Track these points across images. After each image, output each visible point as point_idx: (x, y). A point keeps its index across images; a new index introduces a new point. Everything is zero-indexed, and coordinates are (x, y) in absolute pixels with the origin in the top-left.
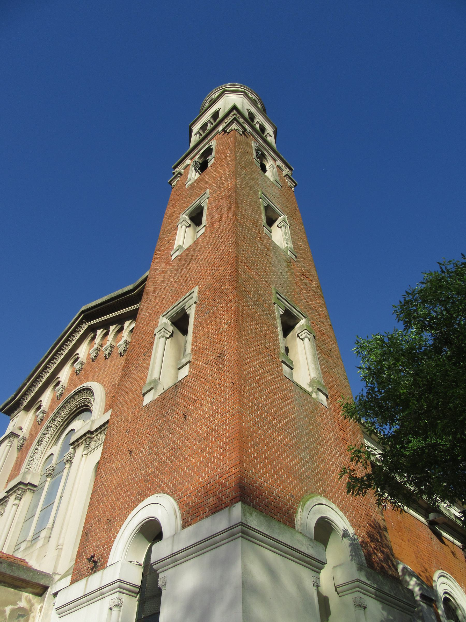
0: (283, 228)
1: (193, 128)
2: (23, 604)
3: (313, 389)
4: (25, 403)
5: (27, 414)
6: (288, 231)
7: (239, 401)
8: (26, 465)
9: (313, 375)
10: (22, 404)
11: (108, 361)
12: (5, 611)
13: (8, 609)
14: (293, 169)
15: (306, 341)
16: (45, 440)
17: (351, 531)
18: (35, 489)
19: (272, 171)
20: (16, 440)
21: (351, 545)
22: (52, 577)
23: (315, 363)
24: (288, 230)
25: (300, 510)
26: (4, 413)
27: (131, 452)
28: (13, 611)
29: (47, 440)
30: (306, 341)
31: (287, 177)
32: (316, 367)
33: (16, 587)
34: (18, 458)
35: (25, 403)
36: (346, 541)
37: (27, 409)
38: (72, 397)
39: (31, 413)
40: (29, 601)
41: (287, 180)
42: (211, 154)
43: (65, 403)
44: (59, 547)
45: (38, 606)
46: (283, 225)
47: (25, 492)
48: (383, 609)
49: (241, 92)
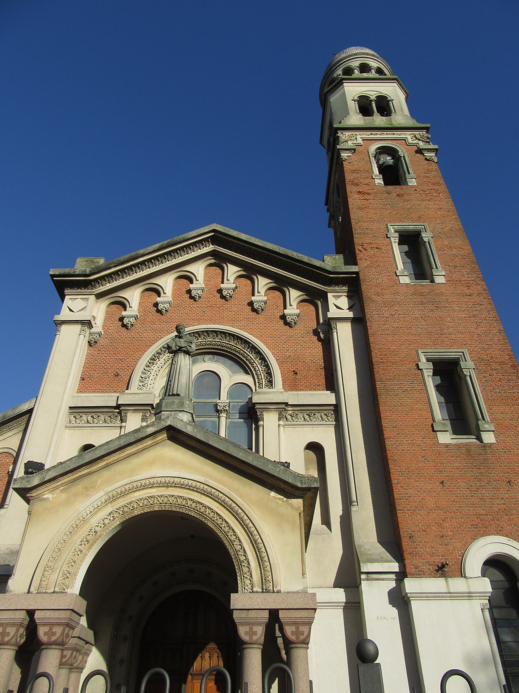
5: (97, 302)
10: (94, 287)
37: (99, 296)
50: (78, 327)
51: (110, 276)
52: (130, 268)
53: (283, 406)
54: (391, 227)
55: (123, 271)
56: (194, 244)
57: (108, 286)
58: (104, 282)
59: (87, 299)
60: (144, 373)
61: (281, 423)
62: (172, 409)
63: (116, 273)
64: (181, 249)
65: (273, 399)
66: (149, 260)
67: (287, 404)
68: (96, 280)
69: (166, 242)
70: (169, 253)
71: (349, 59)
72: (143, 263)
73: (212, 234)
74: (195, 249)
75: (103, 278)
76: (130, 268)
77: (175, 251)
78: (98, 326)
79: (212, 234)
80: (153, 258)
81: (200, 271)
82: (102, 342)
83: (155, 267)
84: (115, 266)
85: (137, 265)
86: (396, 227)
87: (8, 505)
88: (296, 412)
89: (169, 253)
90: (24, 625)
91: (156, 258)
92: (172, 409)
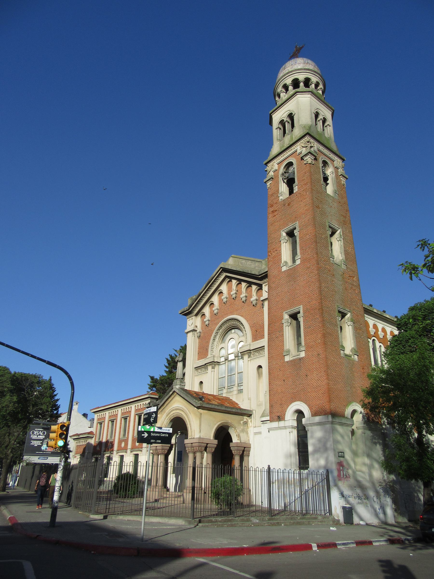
0: (339, 241)
1: (273, 116)
2: (245, 420)
3: (352, 354)
4: (195, 312)
5: (197, 318)
6: (342, 244)
7: (328, 379)
8: (210, 351)
9: (353, 346)
10: (193, 312)
11: (246, 305)
12: (241, 423)
13: (242, 422)
14: (345, 159)
15: (350, 327)
16: (217, 340)
17: (363, 411)
18: (219, 363)
19: (332, 176)
20: (196, 333)
21: (362, 416)
22: (252, 411)
23: (354, 339)
24: (342, 244)
25: (347, 410)
26: (182, 315)
27: (284, 381)
28: (243, 422)
29: (218, 339)
30: (350, 327)
31: (341, 176)
32: (354, 341)
33: (242, 415)
34: (199, 342)
35: (195, 312)
36: (361, 415)
37: (196, 315)
38: (228, 320)
39: (199, 318)
40: (246, 419)
41: (341, 178)
42: (294, 182)
43: (224, 322)
44: (249, 399)
45: (250, 420)
46: (340, 240)
47: (215, 365)
48: (371, 433)
49: (309, 92)
50: (191, 333)
51: (195, 306)
52: (200, 299)
53: (249, 351)
54: (283, 232)
55: (199, 301)
56: (218, 277)
57: (197, 309)
58: (195, 309)
59: (192, 319)
60: (212, 347)
61: (249, 359)
62: (338, 266)
63: (197, 303)
64: (214, 281)
65: (245, 349)
66: (205, 293)
67: (250, 350)
68: (192, 310)
69: (205, 285)
70: (211, 286)
71: (278, 84)
72: (204, 295)
73: (222, 269)
74: (212, 287)
75: (194, 308)
76: (200, 299)
77: (212, 283)
78: (199, 329)
79: (222, 269)
80: (206, 291)
81: (225, 287)
82: (202, 335)
83: (209, 294)
84: (195, 302)
85: (202, 297)
86: (285, 230)
87: (219, 391)
88: (254, 352)
89: (211, 286)
90: (155, 460)
91: (207, 290)
92: (338, 266)
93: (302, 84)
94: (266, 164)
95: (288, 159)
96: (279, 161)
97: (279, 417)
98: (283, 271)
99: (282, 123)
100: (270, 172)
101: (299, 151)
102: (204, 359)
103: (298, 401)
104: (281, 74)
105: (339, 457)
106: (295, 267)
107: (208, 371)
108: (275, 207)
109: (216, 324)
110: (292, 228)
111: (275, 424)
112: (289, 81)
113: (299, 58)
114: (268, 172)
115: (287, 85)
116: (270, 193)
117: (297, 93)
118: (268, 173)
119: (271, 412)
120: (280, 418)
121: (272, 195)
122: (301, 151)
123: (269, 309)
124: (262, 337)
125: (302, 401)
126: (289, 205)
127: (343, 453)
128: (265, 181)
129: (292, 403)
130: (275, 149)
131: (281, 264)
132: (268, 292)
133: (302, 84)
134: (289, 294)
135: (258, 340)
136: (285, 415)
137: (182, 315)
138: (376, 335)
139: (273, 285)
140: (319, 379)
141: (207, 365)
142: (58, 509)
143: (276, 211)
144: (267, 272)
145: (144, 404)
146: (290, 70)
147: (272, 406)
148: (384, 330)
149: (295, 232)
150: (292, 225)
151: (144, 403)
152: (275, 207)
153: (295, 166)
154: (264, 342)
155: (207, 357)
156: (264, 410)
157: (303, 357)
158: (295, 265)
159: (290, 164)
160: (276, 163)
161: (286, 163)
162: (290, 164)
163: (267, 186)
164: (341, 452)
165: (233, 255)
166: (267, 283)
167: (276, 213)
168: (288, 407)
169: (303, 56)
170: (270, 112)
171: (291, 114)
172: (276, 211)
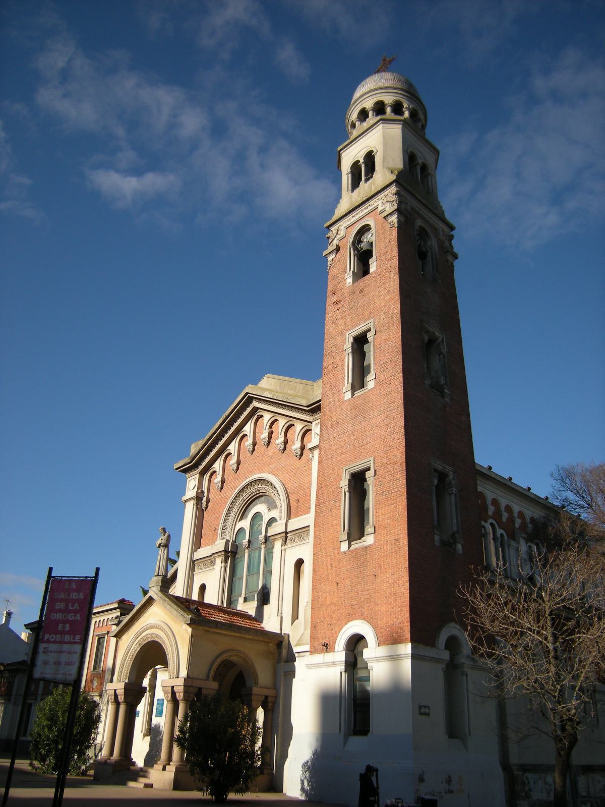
26: (180, 471)
42: (371, 256)
93: (388, 110)
94: (328, 227)
95: (362, 221)
96: (348, 223)
97: (326, 645)
98: (346, 399)
99: (355, 167)
100: (334, 240)
101: (380, 208)
102: (209, 547)
103: (358, 619)
104: (357, 94)
105: (421, 714)
106: (366, 392)
107: (214, 567)
108: (338, 296)
109: (218, 518)
110: (364, 329)
111: (319, 658)
112: (369, 104)
113: (387, 73)
114: (330, 241)
115: (366, 110)
116: (331, 273)
117: (307, 409)
118: (331, 242)
119: (313, 638)
120: (327, 647)
121: (335, 277)
122: (384, 207)
123: (320, 462)
124: (307, 511)
125: (364, 619)
126: (361, 291)
127: (429, 707)
128: (325, 253)
129: (348, 622)
130: (344, 206)
131: (344, 388)
132: (321, 436)
133: (388, 110)
134: (353, 438)
135: (301, 515)
136: (335, 642)
137: (180, 471)
138: (497, 514)
139: (329, 424)
140: (395, 583)
141: (214, 556)
142: (93, 616)
143: (340, 301)
144: (320, 401)
145: (110, 619)
146: (372, 88)
147: (315, 627)
148: (509, 509)
149: (369, 335)
150: (365, 324)
151: (110, 617)
152: (338, 296)
153: (373, 230)
154: (308, 519)
155: (216, 543)
156: (303, 634)
157: (371, 545)
158: (366, 391)
159: (365, 229)
160: (344, 225)
161: (360, 227)
162: (365, 229)
163: (327, 261)
164: (425, 707)
165: (268, 375)
166: (319, 421)
167: (339, 305)
168: (341, 629)
169: (392, 71)
170: (339, 149)
171: (371, 152)
172: (340, 301)
